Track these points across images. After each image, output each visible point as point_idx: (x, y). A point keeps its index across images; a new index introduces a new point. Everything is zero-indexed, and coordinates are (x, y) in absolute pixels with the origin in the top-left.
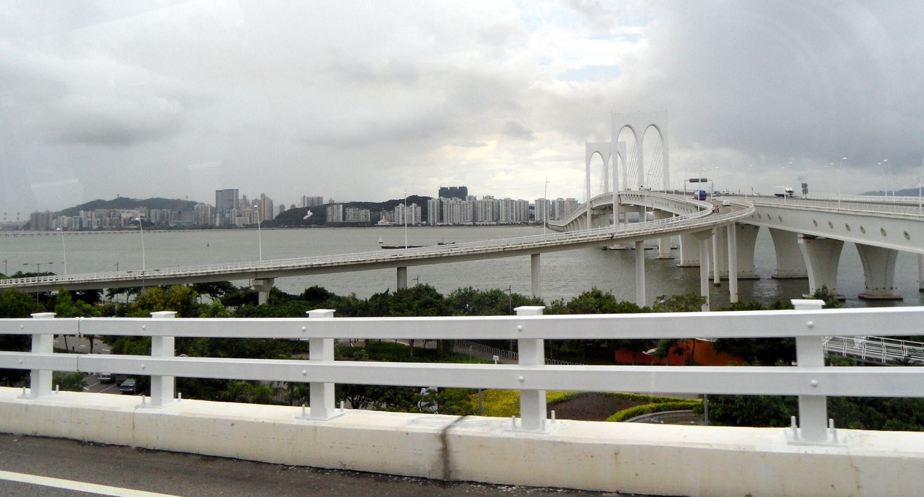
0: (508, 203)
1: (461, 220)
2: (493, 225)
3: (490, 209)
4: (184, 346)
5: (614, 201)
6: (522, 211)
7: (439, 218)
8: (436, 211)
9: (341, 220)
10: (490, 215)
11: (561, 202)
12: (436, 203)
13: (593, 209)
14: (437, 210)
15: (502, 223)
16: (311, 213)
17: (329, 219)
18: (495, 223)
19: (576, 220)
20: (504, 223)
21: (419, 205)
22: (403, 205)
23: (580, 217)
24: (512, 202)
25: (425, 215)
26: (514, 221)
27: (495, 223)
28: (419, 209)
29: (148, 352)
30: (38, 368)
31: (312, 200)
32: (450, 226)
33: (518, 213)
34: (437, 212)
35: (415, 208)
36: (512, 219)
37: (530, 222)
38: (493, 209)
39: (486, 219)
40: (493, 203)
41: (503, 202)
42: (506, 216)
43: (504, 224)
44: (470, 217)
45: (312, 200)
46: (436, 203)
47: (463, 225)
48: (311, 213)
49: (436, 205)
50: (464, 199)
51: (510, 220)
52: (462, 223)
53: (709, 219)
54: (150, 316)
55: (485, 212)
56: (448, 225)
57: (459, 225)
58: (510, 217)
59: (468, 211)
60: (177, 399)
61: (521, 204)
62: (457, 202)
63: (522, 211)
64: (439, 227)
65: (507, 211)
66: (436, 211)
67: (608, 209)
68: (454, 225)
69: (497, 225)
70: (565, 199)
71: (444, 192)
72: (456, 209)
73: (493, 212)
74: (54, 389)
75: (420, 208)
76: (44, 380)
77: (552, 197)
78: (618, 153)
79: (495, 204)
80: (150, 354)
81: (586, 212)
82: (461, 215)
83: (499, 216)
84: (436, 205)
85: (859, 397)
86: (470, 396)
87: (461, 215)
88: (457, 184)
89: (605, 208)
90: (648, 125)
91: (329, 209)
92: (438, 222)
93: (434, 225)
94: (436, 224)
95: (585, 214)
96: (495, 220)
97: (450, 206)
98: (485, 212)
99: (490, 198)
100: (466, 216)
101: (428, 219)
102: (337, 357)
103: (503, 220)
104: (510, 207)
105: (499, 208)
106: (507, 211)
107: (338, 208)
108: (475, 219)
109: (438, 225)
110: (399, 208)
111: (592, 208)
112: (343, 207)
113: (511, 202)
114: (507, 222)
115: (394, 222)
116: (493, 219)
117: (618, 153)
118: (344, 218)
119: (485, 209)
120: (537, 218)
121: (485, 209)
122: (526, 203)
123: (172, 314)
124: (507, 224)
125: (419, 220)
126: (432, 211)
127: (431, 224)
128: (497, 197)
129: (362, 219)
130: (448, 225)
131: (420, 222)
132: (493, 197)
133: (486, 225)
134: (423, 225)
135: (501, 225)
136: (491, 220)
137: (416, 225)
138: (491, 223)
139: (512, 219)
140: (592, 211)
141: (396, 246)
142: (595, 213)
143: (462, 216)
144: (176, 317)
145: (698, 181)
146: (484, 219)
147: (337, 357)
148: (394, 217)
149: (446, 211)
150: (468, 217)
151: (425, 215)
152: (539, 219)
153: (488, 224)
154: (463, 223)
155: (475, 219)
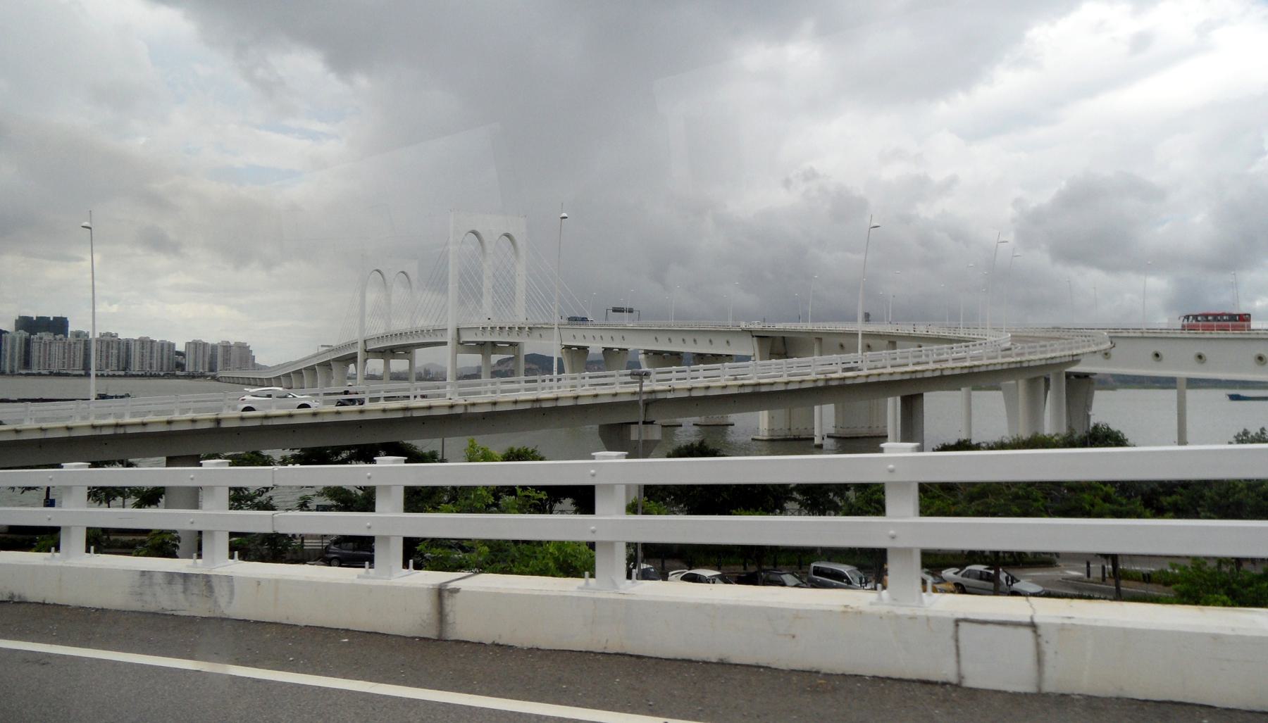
0: (145, 345)
1: (64, 367)
3: (115, 351)
4: (418, 499)
7: (22, 361)
10: (114, 361)
11: (227, 347)
12: (18, 339)
13: (368, 352)
15: (134, 373)
18: (122, 373)
20: (137, 373)
24: (151, 344)
26: (154, 371)
27: (122, 373)
29: (196, 505)
30: (210, 528)
32: (45, 375)
34: (20, 353)
36: (151, 367)
37: (178, 373)
38: (119, 353)
39: (107, 367)
40: (119, 343)
41: (138, 343)
43: (138, 376)
44: (79, 362)
46: (18, 339)
47: (67, 375)
50: (66, 335)
51: (148, 369)
52: (65, 372)
53: (1049, 348)
54: (201, 465)
55: (107, 357)
56: (40, 374)
57: (59, 375)
58: (148, 365)
60: (88, 554)
61: (165, 346)
62: (55, 339)
64: (23, 377)
65: (142, 356)
67: (388, 351)
68: (51, 374)
69: (126, 376)
70: (232, 343)
71: (27, 324)
73: (119, 356)
74: (88, 551)
76: (74, 542)
77: (212, 338)
80: (373, 510)
82: (64, 358)
85: (768, 546)
87: (64, 358)
88: (51, 313)
89: (385, 351)
92: (19, 368)
93: (12, 374)
94: (16, 372)
96: (121, 368)
97: (45, 344)
98: (107, 357)
99: (111, 335)
100: (74, 360)
102: (925, 511)
103: (135, 368)
104: (149, 350)
106: (142, 356)
109: (21, 374)
111: (365, 351)
113: (149, 343)
114: (143, 373)
116: (118, 366)
119: (108, 352)
121: (108, 352)
122: (171, 346)
123: (86, 465)
124: (142, 376)
127: (8, 370)
128: (122, 336)
130: (40, 374)
132: (117, 334)
133: (108, 376)
136: (116, 369)
138: (117, 373)
139: (151, 367)
140: (366, 353)
141: (11, 398)
143: (66, 360)
144: (230, 466)
145: (623, 312)
146: (104, 367)
147: (925, 511)
150: (77, 362)
152: (191, 370)
153: (110, 373)
154: (69, 372)
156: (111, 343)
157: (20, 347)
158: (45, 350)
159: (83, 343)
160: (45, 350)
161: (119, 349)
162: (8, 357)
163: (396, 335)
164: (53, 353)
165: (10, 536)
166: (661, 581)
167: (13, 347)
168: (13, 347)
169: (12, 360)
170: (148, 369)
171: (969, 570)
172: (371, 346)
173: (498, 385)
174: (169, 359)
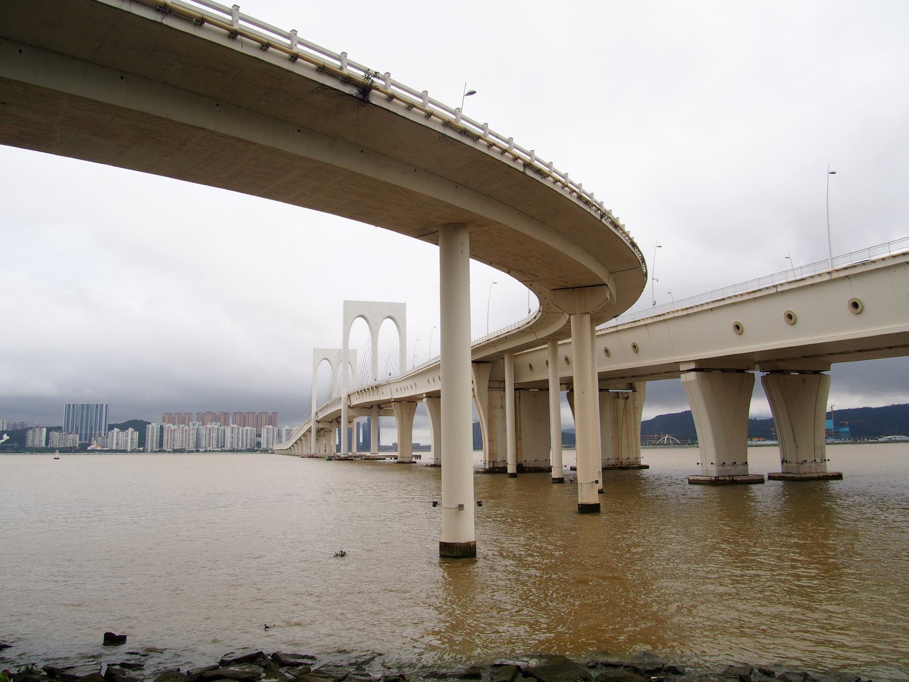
2: (218, 451)
5: (342, 406)
6: (249, 441)
7: (158, 443)
8: (155, 439)
9: (44, 445)
12: (155, 428)
13: (319, 422)
14: (157, 436)
16: (8, 437)
17: (29, 443)
19: (300, 439)
21: (136, 430)
22: (118, 430)
23: (304, 435)
25: (142, 442)
27: (220, 450)
28: (136, 434)
31: (15, 424)
32: (169, 452)
33: (245, 441)
35: (132, 432)
36: (238, 446)
38: (218, 435)
39: (209, 446)
42: (232, 443)
45: (15, 424)
46: (155, 428)
48: (8, 437)
49: (155, 430)
51: (236, 447)
59: (191, 437)
62: (179, 428)
63: (249, 441)
66: (155, 439)
67: (375, 407)
72: (178, 435)
73: (218, 439)
75: (138, 433)
78: (349, 363)
79: (220, 431)
81: (310, 428)
83: (224, 442)
84: (155, 430)
86: (364, 667)
89: (332, 421)
90: (385, 316)
91: (30, 433)
92: (156, 448)
95: (309, 431)
97: (171, 431)
101: (146, 445)
103: (228, 446)
105: (224, 438)
107: (41, 431)
108: (198, 445)
110: (113, 433)
111: (349, 407)
112: (47, 431)
115: (107, 447)
116: (218, 445)
117: (349, 363)
118: (47, 444)
120: (264, 446)
125: (136, 447)
126: (152, 431)
129: (69, 444)
131: (137, 449)
134: (139, 452)
135: (226, 451)
137: (132, 451)
138: (215, 449)
139: (238, 446)
142: (321, 426)
148: (107, 442)
149: (166, 435)
150: (191, 443)
151: (142, 442)
155: (198, 445)
156: (212, 429)
157: (157, 433)
158: (171, 435)
159: (195, 430)
160: (171, 435)
161: (218, 433)
162: (150, 441)
163: (364, 390)
164: (176, 436)
165: (472, 670)
166: (873, 407)
167: (153, 433)
168: (153, 433)
169: (152, 443)
170: (236, 447)
171: (276, 679)
172: (355, 401)
173: (738, 571)
174: (251, 439)
